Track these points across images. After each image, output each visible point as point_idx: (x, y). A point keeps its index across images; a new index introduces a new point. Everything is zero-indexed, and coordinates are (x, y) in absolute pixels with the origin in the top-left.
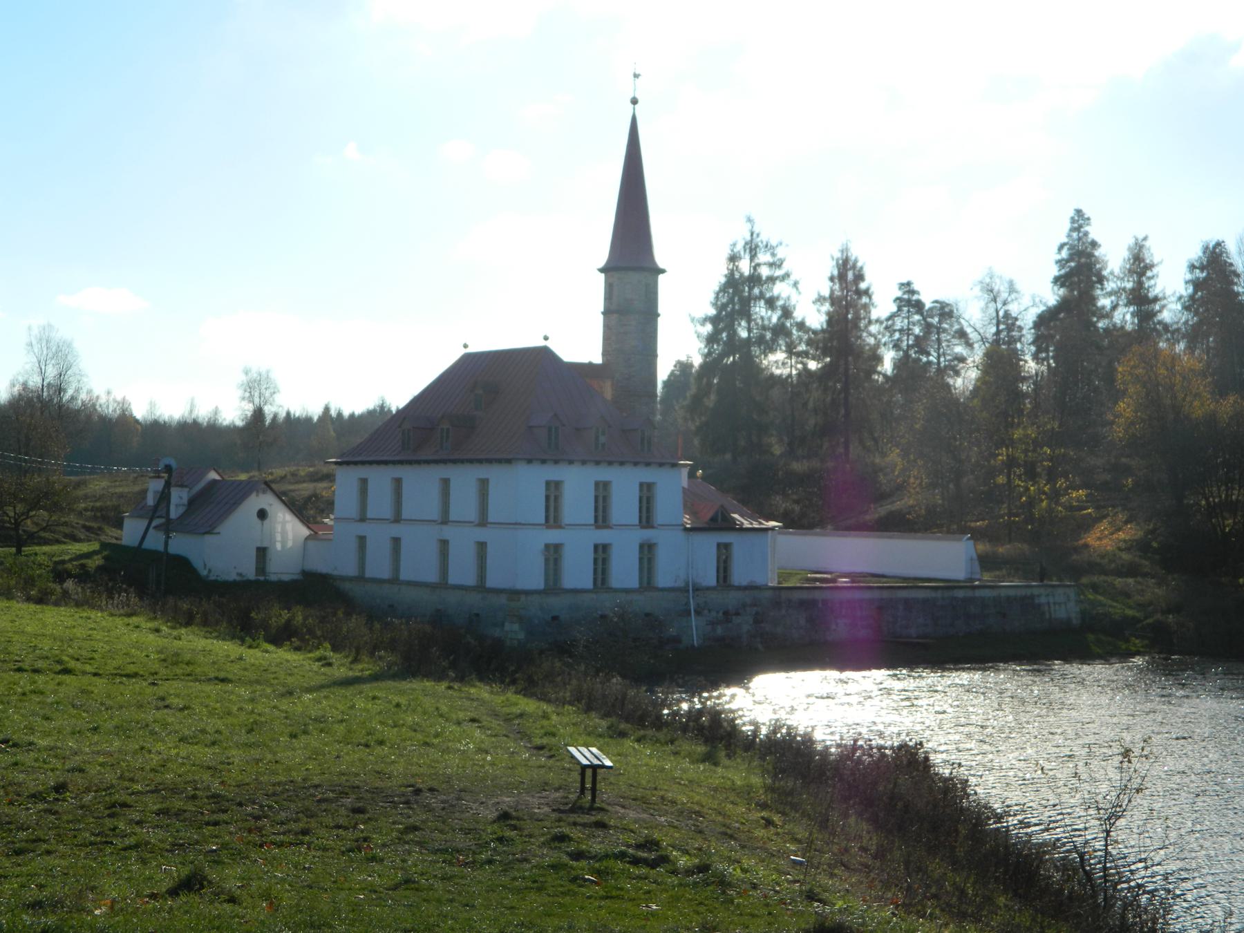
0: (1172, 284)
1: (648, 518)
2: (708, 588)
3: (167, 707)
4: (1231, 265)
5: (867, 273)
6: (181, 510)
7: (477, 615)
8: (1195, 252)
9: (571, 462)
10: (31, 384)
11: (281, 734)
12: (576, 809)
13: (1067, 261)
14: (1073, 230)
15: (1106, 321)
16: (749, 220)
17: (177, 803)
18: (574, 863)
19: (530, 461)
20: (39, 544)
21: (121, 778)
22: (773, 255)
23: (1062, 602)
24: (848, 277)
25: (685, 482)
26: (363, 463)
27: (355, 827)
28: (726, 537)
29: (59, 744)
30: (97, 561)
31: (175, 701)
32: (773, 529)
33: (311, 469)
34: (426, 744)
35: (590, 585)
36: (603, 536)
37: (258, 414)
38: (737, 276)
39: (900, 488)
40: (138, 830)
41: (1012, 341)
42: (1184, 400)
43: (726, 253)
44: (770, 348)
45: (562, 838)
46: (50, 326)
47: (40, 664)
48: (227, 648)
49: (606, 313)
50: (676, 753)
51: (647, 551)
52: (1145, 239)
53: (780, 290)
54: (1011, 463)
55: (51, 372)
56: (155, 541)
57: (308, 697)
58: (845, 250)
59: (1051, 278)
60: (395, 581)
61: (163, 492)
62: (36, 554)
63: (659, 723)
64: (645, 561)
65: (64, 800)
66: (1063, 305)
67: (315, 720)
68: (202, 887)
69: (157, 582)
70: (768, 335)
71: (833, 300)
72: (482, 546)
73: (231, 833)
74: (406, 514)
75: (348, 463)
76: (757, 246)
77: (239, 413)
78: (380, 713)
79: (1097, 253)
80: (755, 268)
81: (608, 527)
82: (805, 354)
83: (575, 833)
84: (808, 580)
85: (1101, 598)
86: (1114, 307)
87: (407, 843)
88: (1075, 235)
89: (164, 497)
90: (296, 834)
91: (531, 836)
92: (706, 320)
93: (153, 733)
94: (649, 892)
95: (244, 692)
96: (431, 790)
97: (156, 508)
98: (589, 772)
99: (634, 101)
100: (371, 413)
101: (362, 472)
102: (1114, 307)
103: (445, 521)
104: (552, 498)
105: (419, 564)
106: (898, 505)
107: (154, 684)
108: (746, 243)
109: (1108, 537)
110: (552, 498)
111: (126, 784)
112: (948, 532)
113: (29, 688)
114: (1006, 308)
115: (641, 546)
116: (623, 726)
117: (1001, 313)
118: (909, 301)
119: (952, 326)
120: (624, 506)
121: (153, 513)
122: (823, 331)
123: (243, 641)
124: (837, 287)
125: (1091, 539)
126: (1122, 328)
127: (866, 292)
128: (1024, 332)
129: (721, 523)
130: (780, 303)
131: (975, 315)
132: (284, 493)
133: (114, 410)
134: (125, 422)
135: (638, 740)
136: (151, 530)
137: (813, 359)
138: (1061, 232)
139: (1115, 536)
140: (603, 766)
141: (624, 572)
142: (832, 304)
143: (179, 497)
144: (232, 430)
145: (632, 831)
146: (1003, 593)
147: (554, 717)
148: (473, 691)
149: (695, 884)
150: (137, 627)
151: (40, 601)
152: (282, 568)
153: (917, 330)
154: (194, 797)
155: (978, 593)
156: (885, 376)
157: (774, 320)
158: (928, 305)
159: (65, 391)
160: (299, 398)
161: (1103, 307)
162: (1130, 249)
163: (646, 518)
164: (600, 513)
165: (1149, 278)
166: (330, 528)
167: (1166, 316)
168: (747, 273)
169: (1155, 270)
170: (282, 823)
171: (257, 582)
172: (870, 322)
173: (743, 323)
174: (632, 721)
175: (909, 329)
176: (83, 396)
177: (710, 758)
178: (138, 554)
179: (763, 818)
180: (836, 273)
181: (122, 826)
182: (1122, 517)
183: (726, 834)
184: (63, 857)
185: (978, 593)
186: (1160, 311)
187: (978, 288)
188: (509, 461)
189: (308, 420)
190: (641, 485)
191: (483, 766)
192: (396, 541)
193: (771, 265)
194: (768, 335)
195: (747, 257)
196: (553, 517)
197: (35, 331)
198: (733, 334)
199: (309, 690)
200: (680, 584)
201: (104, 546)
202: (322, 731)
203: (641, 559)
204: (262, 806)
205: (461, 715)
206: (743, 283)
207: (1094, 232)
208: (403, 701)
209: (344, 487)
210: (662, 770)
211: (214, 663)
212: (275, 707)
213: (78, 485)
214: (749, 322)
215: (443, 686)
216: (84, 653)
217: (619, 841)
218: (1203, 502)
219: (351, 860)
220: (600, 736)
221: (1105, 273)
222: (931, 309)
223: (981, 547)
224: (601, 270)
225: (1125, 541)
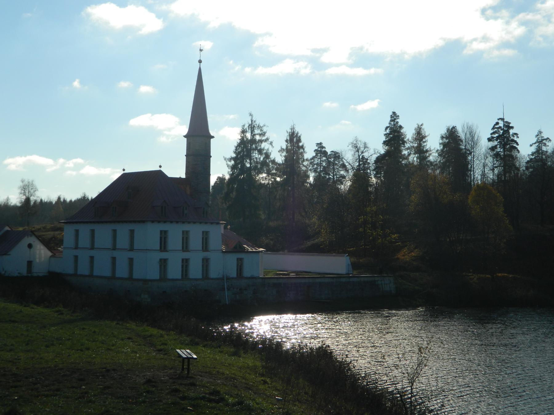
0: (434, 144)
1: (206, 247)
2: (233, 278)
4: (459, 136)
5: (302, 139)
8: (444, 131)
13: (389, 134)
15: (406, 161)
16: (251, 115)
18: (183, 402)
19: (153, 222)
22: (261, 130)
23: (388, 283)
24: (294, 139)
25: (222, 231)
26: (77, 223)
32: (262, 251)
35: (180, 277)
37: (28, 200)
38: (245, 139)
41: (365, 169)
44: (260, 172)
45: (176, 391)
48: (14, 307)
51: (206, 262)
52: (422, 125)
53: (264, 145)
58: (293, 129)
60: (91, 276)
63: (213, 339)
66: (387, 153)
70: (259, 166)
71: (287, 150)
72: (131, 260)
76: (254, 126)
77: (19, 200)
79: (402, 131)
81: (167, 251)
82: (275, 174)
88: (392, 123)
92: (231, 159)
96: (114, 370)
99: (200, 62)
100: (79, 201)
101: (77, 227)
102: (409, 155)
103: (114, 248)
104: (185, 238)
105: (102, 268)
110: (185, 238)
114: (363, 154)
115: (203, 260)
117: (361, 157)
118: (320, 150)
119: (339, 162)
120: (195, 242)
125: (400, 256)
126: (413, 163)
127: (302, 147)
128: (371, 165)
131: (349, 157)
135: (204, 346)
139: (410, 254)
140: (193, 358)
141: (195, 271)
142: (287, 153)
144: (15, 207)
147: (166, 336)
149: (237, 410)
152: (39, 270)
153: (324, 164)
155: (351, 280)
156: (310, 184)
157: (262, 159)
158: (329, 153)
160: (46, 193)
161: (405, 155)
162: (415, 129)
163: (205, 247)
166: (61, 252)
167: (431, 158)
172: (304, 161)
173: (248, 161)
174: (199, 338)
177: (235, 354)
179: (262, 380)
180: (288, 138)
185: (351, 280)
186: (429, 156)
187: (350, 146)
188: (144, 222)
189: (51, 203)
190: (203, 232)
192: (131, 260)
193: (260, 135)
194: (259, 166)
195: (250, 131)
196: (163, 247)
198: (243, 165)
202: (60, 344)
203: (203, 266)
206: (248, 143)
207: (401, 122)
209: (68, 233)
212: (38, 333)
214: (250, 160)
215: (115, 323)
221: (405, 140)
225: (414, 256)
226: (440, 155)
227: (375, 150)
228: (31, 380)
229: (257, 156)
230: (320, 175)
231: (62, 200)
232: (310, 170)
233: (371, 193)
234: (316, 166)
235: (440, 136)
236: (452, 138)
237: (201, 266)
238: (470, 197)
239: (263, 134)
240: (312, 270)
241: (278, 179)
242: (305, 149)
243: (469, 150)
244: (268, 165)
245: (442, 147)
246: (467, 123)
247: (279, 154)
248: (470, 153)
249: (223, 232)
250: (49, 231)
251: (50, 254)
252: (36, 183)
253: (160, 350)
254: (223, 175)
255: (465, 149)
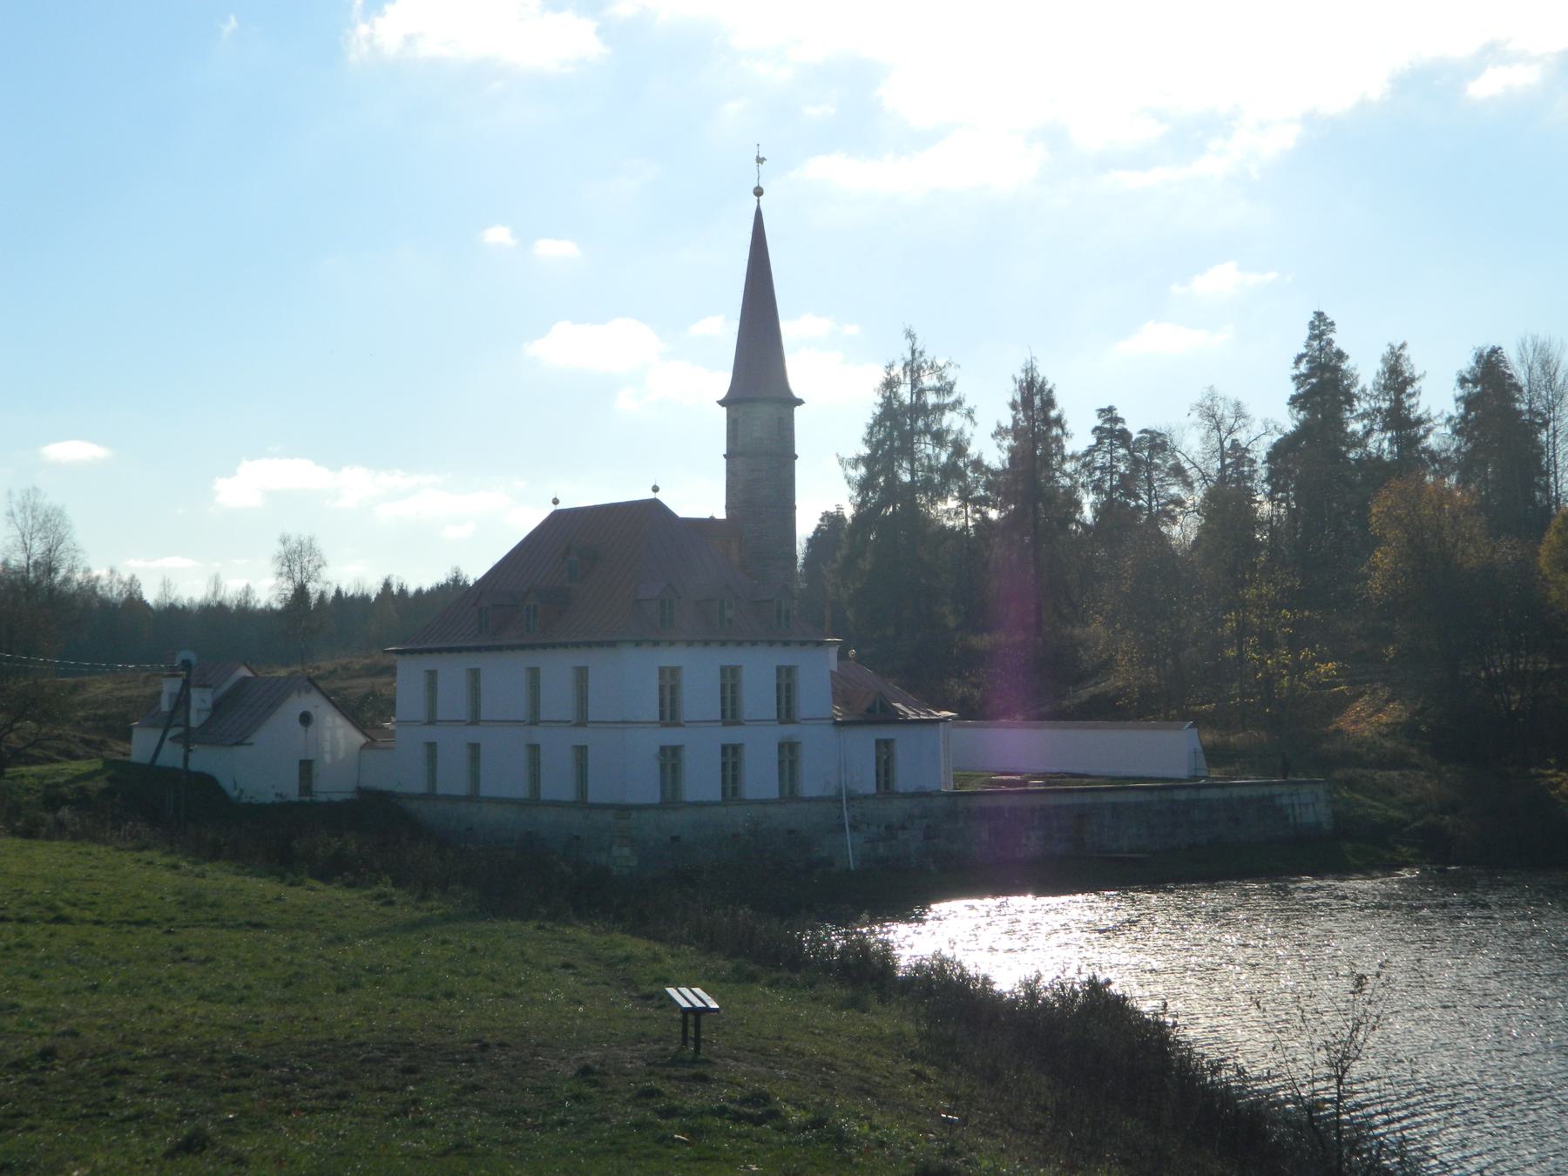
0: (1438, 400)
1: (788, 710)
2: (866, 797)
3: (185, 959)
4: (1511, 376)
5: (1058, 396)
6: (204, 717)
7: (577, 838)
8: (1466, 363)
9: (672, 643)
10: (13, 563)
11: (327, 987)
12: (677, 1061)
13: (1307, 376)
14: (1312, 337)
15: (1359, 450)
16: (910, 335)
17: (190, 1068)
18: (663, 1122)
19: (638, 644)
20: (27, 764)
21: (123, 1041)
22: (940, 378)
23: (1310, 804)
24: (1035, 401)
25: (833, 663)
26: (430, 651)
27: (403, 1089)
28: (885, 733)
29: (49, 1006)
30: (101, 783)
31: (196, 952)
32: (945, 720)
33: (367, 661)
34: (506, 995)
36: (733, 735)
37: (301, 592)
38: (896, 405)
39: (1107, 666)
40: (139, 1099)
41: (1243, 478)
42: (1455, 546)
43: (880, 376)
44: (940, 493)
45: (651, 1093)
46: (35, 489)
47: (27, 912)
48: (259, 887)
49: (729, 456)
50: (815, 999)
51: (788, 753)
52: (1403, 346)
53: (952, 421)
54: (1243, 630)
55: (38, 548)
56: (172, 756)
57: (361, 943)
58: (1030, 370)
59: (1287, 399)
60: (473, 798)
61: (180, 695)
62: (23, 776)
63: (796, 960)
64: (787, 764)
65: (53, 1069)
66: (1303, 431)
67: (370, 970)
68: (204, 1148)
69: (178, 811)
70: (937, 478)
71: (1016, 431)
72: (581, 751)
73: (252, 1100)
74: (484, 714)
75: (412, 652)
76: (920, 367)
77: (275, 593)
78: (451, 959)
79: (1344, 366)
80: (919, 397)
82: (983, 501)
83: (667, 1088)
84: (992, 783)
85: (1358, 796)
86: (1368, 433)
87: (465, 1104)
88: (1315, 343)
89: (182, 701)
90: (332, 1098)
91: (614, 1092)
92: (856, 463)
93: (166, 990)
94: (749, 1152)
95: (283, 940)
96: (502, 1045)
97: (172, 713)
98: (691, 1017)
99: (758, 192)
100: (441, 590)
101: (430, 662)
102: (1368, 433)
103: (535, 721)
105: (504, 778)
106: (1114, 682)
107: (169, 932)
108: (906, 365)
109: (1368, 718)
111: (129, 1047)
112: (1167, 719)
113: (14, 940)
114: (1233, 437)
115: (781, 746)
116: (751, 968)
117: (1227, 444)
118: (1111, 430)
119: (1165, 461)
120: (758, 695)
121: (169, 721)
122: (1005, 470)
123: (282, 879)
124: (1021, 415)
126: (1379, 458)
127: (1058, 422)
128: (1256, 466)
129: (879, 714)
130: (951, 437)
131: (1192, 444)
132: (335, 692)
133: (120, 594)
134: (134, 604)
135: (771, 985)
136: (167, 744)
137: (994, 507)
138: (1297, 340)
140: (707, 1010)
141: (760, 780)
142: (1015, 439)
143: (201, 701)
144: (268, 614)
145: (739, 1085)
146: (1236, 792)
147: (669, 961)
148: (569, 931)
149: (807, 1142)
150: (150, 863)
151: (29, 833)
152: (333, 785)
153: (1122, 468)
154: (211, 1061)
155: (1204, 794)
156: (1084, 525)
157: (944, 458)
158: (1135, 436)
159: (56, 570)
160: (350, 572)
161: (1354, 433)
162: (1384, 360)
163: (786, 711)
164: (729, 707)
165: (1410, 396)
166: (391, 734)
167: (1432, 442)
168: (908, 401)
169: (1416, 385)
170: (315, 1087)
171: (301, 804)
172: (1064, 459)
174: (760, 959)
175: (1112, 467)
176: (79, 576)
177: (854, 1003)
178: (151, 772)
179: (913, 1071)
180: (1018, 398)
181: (120, 1096)
182: (1383, 693)
183: (861, 1089)
184: (49, 1131)
185: (1204, 794)
186: (1425, 437)
187: (1195, 415)
188: (612, 644)
189: (365, 599)
190: (779, 669)
191: (572, 1019)
192: (475, 748)
193: (938, 391)
194: (937, 478)
195: (908, 380)
196: (670, 714)
197: (17, 497)
198: (893, 478)
199: (365, 936)
200: (831, 792)
201: (109, 763)
202: (377, 983)
203: (781, 763)
204: (292, 1069)
205: (552, 960)
206: (904, 415)
207: (1339, 340)
208: (479, 944)
209: (409, 680)
210: (796, 1018)
211: (245, 904)
212: (320, 956)
213: (75, 688)
214: (912, 463)
215: (531, 926)
216: (83, 897)
217: (723, 1095)
218: (1483, 674)
219: (395, 1126)
220: (723, 981)
221: (1354, 390)
222: (1139, 440)
223: (1208, 737)
224: (722, 403)
225: (1387, 725)
226: (1457, 432)
227: (1266, 423)
228: (277, 1072)
229: (929, 450)
230: (1111, 500)
231: (395, 589)
232: (1083, 485)
233: (1258, 546)
234: (1098, 473)
235: (1455, 378)
236: (1489, 381)
237: (719, 768)
238: (1544, 550)
239: (945, 389)
240: (1146, 773)
241: (993, 514)
242: (1068, 427)
243: (1540, 414)
244: (962, 476)
245: (1461, 411)
246: (1534, 338)
247: (994, 443)
248: (1546, 424)
249: (835, 669)
250: (359, 677)
251: (361, 740)
252: (322, 545)
253: (650, 997)
254: (839, 508)
255: (1530, 411)
